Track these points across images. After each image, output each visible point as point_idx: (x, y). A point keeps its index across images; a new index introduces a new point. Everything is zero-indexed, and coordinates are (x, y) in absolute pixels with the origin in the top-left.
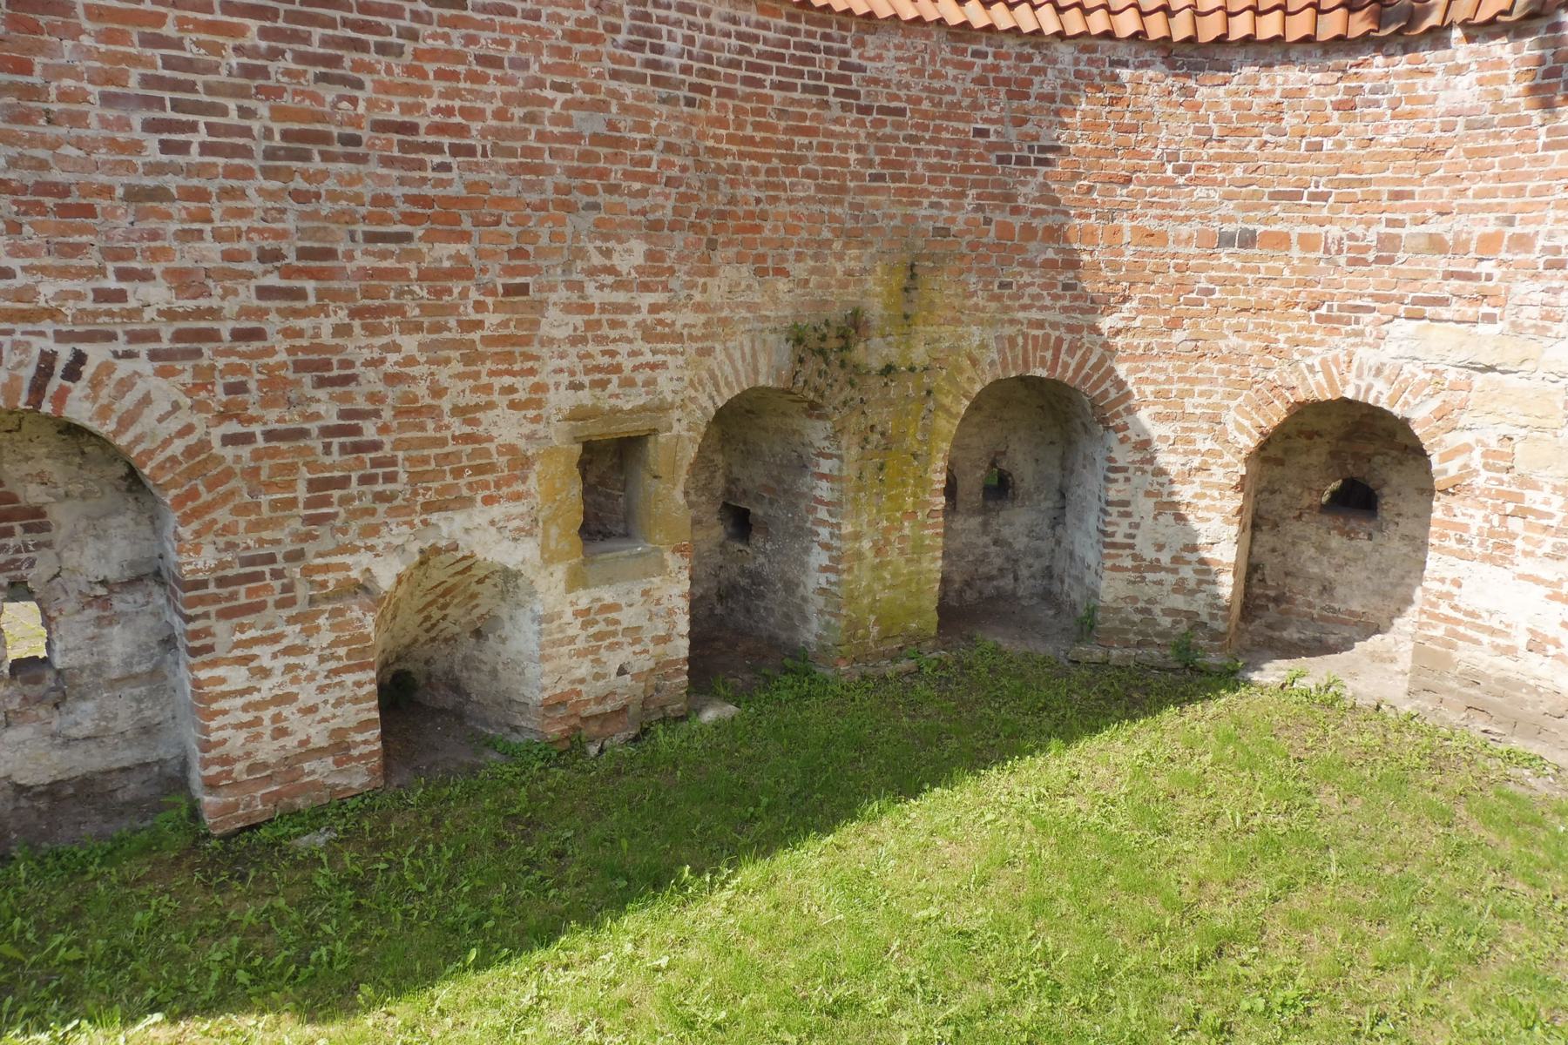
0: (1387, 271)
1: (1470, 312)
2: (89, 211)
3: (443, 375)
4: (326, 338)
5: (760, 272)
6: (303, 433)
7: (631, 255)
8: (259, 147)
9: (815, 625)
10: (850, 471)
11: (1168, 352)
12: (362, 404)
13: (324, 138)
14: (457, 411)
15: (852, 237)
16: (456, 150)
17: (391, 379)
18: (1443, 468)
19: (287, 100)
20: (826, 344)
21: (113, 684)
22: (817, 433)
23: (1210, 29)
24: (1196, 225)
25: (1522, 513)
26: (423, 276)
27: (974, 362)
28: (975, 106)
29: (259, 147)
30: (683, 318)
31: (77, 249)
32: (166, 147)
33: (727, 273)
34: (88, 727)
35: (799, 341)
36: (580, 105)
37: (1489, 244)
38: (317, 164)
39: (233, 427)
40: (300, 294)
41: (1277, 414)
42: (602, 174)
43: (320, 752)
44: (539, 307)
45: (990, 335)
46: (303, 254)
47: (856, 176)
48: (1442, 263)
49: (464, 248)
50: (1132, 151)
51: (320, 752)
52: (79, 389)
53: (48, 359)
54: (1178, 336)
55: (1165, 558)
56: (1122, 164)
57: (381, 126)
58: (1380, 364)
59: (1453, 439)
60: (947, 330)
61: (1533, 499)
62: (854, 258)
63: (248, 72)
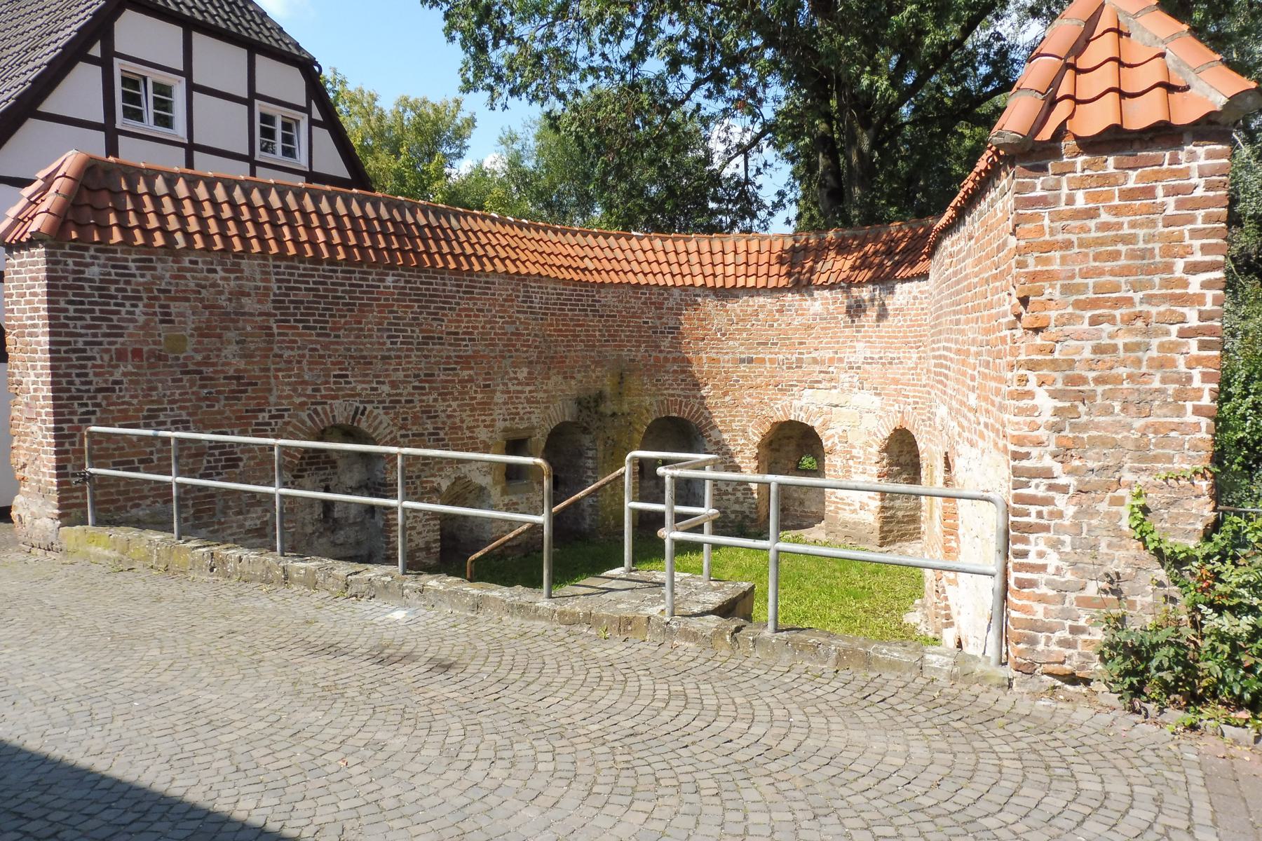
0: (800, 371)
1: (828, 385)
2: (371, 363)
3: (464, 415)
4: (431, 403)
5: (565, 378)
6: (423, 435)
7: (523, 373)
8: (415, 342)
9: (588, 521)
10: (600, 455)
11: (724, 405)
12: (440, 425)
13: (433, 338)
14: (468, 428)
15: (598, 363)
16: (470, 340)
17: (449, 417)
18: (827, 444)
19: (424, 327)
20: (590, 404)
21: (350, 525)
22: (586, 440)
23: (730, 283)
24: (731, 356)
25: (852, 458)
26: (460, 382)
27: (648, 411)
28: (643, 313)
29: (415, 342)
30: (540, 395)
31: (367, 375)
32: (392, 343)
33: (554, 378)
34: (341, 540)
35: (579, 403)
36: (507, 323)
37: (831, 360)
38: (431, 346)
39: (403, 432)
40: (424, 388)
41: (767, 427)
42: (514, 346)
43: (421, 550)
44: (494, 391)
45: (653, 400)
46: (426, 375)
47: (599, 341)
48: (818, 368)
49: (471, 372)
50: (705, 329)
51: (421, 550)
52: (364, 419)
53: (357, 408)
54: (727, 398)
55: (730, 489)
56: (701, 332)
57: (449, 333)
58: (802, 406)
59: (829, 433)
60: (636, 399)
61: (855, 452)
62: (599, 372)
63: (414, 319)
